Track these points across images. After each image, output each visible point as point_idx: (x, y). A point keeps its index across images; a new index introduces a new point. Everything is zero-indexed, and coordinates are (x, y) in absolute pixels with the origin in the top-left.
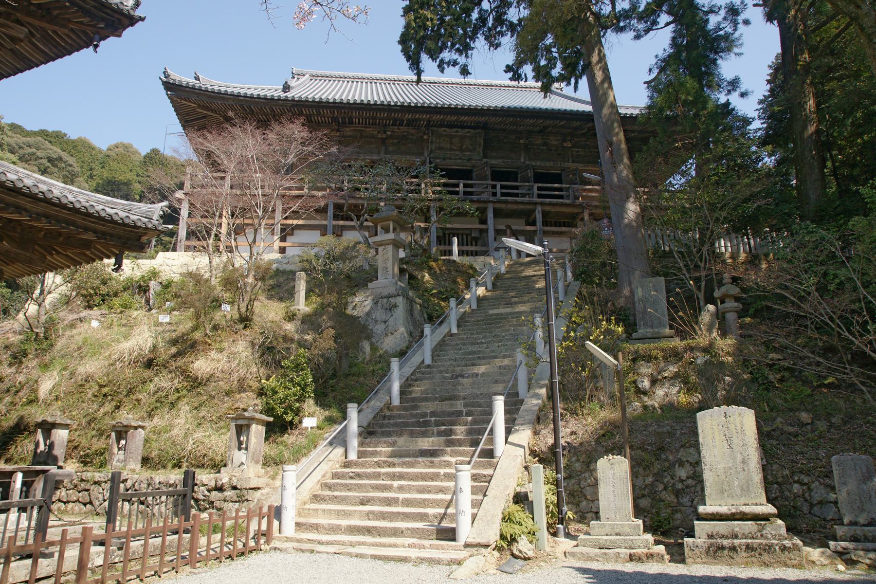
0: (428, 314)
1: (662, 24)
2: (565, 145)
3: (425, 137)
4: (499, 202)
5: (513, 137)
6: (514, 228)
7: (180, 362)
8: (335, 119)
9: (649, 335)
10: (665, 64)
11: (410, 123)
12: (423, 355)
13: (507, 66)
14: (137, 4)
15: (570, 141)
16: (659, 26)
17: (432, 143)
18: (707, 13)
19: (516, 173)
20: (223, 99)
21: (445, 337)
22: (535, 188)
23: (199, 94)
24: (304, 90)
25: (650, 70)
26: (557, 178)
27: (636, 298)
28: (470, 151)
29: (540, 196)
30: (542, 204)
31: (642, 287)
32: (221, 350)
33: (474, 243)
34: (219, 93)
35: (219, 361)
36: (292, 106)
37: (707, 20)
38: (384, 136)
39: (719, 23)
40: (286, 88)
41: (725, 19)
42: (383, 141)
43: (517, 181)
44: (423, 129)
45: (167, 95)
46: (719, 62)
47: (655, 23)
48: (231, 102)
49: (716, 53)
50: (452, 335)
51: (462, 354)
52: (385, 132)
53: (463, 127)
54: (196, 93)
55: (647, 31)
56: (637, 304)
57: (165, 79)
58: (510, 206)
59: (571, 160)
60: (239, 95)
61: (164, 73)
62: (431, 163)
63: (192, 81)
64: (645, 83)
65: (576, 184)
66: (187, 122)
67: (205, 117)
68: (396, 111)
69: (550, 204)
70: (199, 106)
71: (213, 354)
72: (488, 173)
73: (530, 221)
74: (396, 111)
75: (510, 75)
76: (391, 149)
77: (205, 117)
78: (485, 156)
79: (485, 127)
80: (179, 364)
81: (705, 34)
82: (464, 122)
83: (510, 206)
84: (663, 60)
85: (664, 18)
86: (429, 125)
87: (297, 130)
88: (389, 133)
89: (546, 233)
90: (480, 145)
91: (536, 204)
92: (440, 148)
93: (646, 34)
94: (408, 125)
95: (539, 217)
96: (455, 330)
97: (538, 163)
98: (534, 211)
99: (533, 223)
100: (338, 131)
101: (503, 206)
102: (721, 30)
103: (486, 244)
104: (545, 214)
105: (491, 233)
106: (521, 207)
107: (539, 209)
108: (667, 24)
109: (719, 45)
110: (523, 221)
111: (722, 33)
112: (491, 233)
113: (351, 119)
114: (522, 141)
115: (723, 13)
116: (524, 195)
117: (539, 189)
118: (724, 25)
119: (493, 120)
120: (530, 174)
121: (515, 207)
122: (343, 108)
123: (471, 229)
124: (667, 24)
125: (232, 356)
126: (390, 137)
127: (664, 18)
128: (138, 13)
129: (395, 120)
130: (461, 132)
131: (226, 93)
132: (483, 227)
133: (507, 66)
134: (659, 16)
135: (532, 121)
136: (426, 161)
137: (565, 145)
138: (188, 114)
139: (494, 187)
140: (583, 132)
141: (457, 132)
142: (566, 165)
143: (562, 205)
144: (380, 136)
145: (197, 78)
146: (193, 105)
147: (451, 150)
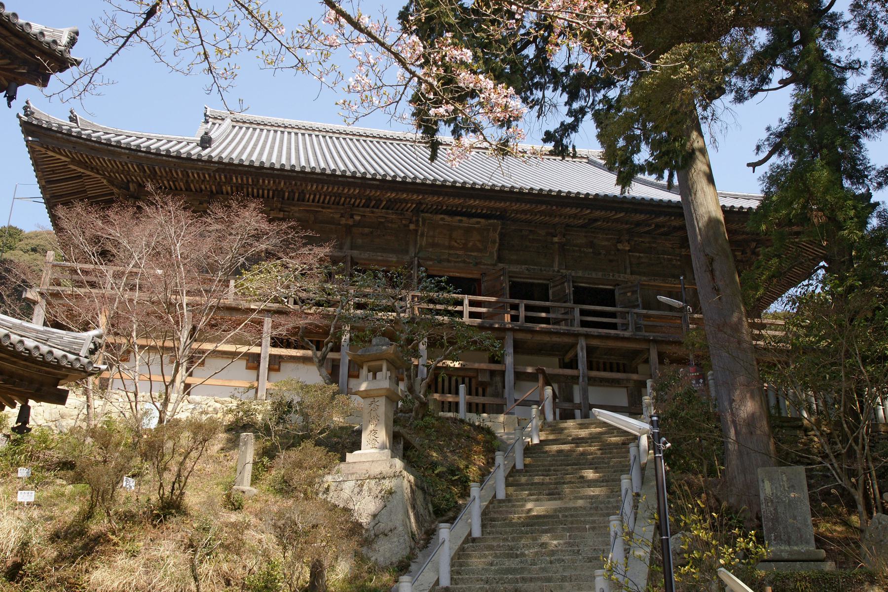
0: (434, 506)
1: (775, 84)
2: (620, 246)
3: (412, 227)
4: (522, 330)
5: (542, 232)
6: (548, 370)
7: (67, 571)
8: (279, 193)
9: (785, 556)
10: (782, 141)
11: (391, 205)
12: (437, 571)
13: (547, 133)
14: (72, 42)
15: (628, 241)
16: (771, 86)
17: (422, 235)
18: (844, 69)
19: (546, 288)
20: (113, 153)
21: (464, 543)
22: (577, 313)
23: (76, 143)
24: (234, 146)
25: (758, 148)
26: (607, 298)
27: (762, 497)
28: (479, 250)
29: (584, 324)
30: (587, 336)
31: (771, 480)
32: (133, 555)
33: (480, 390)
34: (108, 144)
35: (132, 571)
36: (218, 170)
37: (843, 81)
38: (350, 222)
39: (864, 87)
40: (206, 141)
41: (872, 80)
42: (349, 229)
43: (547, 299)
44: (409, 213)
45: (27, 141)
46: (864, 141)
47: (765, 80)
48: (125, 159)
49: (860, 129)
50: (474, 540)
51: (497, 572)
52: (352, 216)
53: (470, 215)
54: (71, 142)
55: (754, 92)
56: (763, 506)
57: (25, 119)
58: (538, 338)
59: (628, 271)
60: (138, 150)
61: (25, 108)
62: (419, 265)
63: (66, 122)
64: (749, 165)
65: (637, 306)
66: (49, 182)
67: (80, 177)
68: (371, 187)
69: (599, 337)
70: (73, 161)
71: (121, 560)
72: (506, 285)
73: (567, 360)
74: (371, 187)
75: (550, 146)
76: (360, 241)
77: (80, 177)
78: (500, 259)
79: (502, 216)
80: (62, 573)
81: (845, 101)
82: (473, 207)
83: (538, 338)
84: (779, 135)
85: (779, 74)
86: (419, 209)
87: (250, 218)
88: (357, 218)
89: (592, 381)
90: (494, 242)
91: (577, 335)
92: (434, 245)
93: (752, 96)
94: (387, 207)
95: (582, 355)
96: (477, 533)
97: (580, 274)
98: (574, 346)
99: (573, 364)
100: (280, 210)
101: (528, 337)
102: (866, 96)
103: (499, 394)
104: (590, 350)
105: (510, 377)
106: (556, 339)
107: (582, 343)
108: (784, 83)
109: (863, 117)
110: (556, 360)
111: (869, 100)
112: (510, 377)
113: (302, 193)
114: (556, 239)
115: (869, 72)
116: (557, 322)
117: (583, 313)
118: (872, 90)
119: (515, 206)
120: (569, 289)
121: (546, 339)
122: (294, 178)
123: (477, 370)
124: (784, 83)
125: (151, 565)
126: (358, 224)
127: (779, 74)
128: (74, 54)
129: (369, 199)
130: (466, 222)
131: (118, 145)
132: (494, 367)
133: (547, 133)
134: (771, 71)
135: (574, 211)
136: (412, 263)
137: (620, 246)
138: (53, 172)
139: (515, 307)
140: (647, 229)
141: (460, 221)
142: (622, 277)
143: (617, 338)
144: (343, 221)
145: (73, 119)
146: (64, 159)
147: (450, 247)
